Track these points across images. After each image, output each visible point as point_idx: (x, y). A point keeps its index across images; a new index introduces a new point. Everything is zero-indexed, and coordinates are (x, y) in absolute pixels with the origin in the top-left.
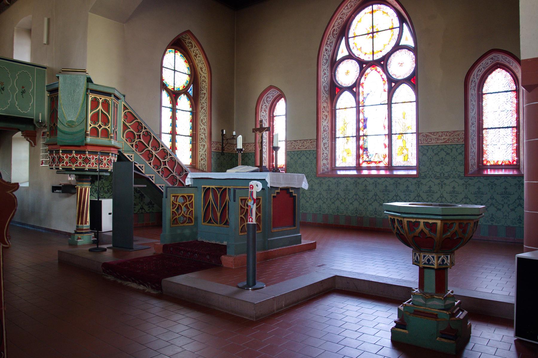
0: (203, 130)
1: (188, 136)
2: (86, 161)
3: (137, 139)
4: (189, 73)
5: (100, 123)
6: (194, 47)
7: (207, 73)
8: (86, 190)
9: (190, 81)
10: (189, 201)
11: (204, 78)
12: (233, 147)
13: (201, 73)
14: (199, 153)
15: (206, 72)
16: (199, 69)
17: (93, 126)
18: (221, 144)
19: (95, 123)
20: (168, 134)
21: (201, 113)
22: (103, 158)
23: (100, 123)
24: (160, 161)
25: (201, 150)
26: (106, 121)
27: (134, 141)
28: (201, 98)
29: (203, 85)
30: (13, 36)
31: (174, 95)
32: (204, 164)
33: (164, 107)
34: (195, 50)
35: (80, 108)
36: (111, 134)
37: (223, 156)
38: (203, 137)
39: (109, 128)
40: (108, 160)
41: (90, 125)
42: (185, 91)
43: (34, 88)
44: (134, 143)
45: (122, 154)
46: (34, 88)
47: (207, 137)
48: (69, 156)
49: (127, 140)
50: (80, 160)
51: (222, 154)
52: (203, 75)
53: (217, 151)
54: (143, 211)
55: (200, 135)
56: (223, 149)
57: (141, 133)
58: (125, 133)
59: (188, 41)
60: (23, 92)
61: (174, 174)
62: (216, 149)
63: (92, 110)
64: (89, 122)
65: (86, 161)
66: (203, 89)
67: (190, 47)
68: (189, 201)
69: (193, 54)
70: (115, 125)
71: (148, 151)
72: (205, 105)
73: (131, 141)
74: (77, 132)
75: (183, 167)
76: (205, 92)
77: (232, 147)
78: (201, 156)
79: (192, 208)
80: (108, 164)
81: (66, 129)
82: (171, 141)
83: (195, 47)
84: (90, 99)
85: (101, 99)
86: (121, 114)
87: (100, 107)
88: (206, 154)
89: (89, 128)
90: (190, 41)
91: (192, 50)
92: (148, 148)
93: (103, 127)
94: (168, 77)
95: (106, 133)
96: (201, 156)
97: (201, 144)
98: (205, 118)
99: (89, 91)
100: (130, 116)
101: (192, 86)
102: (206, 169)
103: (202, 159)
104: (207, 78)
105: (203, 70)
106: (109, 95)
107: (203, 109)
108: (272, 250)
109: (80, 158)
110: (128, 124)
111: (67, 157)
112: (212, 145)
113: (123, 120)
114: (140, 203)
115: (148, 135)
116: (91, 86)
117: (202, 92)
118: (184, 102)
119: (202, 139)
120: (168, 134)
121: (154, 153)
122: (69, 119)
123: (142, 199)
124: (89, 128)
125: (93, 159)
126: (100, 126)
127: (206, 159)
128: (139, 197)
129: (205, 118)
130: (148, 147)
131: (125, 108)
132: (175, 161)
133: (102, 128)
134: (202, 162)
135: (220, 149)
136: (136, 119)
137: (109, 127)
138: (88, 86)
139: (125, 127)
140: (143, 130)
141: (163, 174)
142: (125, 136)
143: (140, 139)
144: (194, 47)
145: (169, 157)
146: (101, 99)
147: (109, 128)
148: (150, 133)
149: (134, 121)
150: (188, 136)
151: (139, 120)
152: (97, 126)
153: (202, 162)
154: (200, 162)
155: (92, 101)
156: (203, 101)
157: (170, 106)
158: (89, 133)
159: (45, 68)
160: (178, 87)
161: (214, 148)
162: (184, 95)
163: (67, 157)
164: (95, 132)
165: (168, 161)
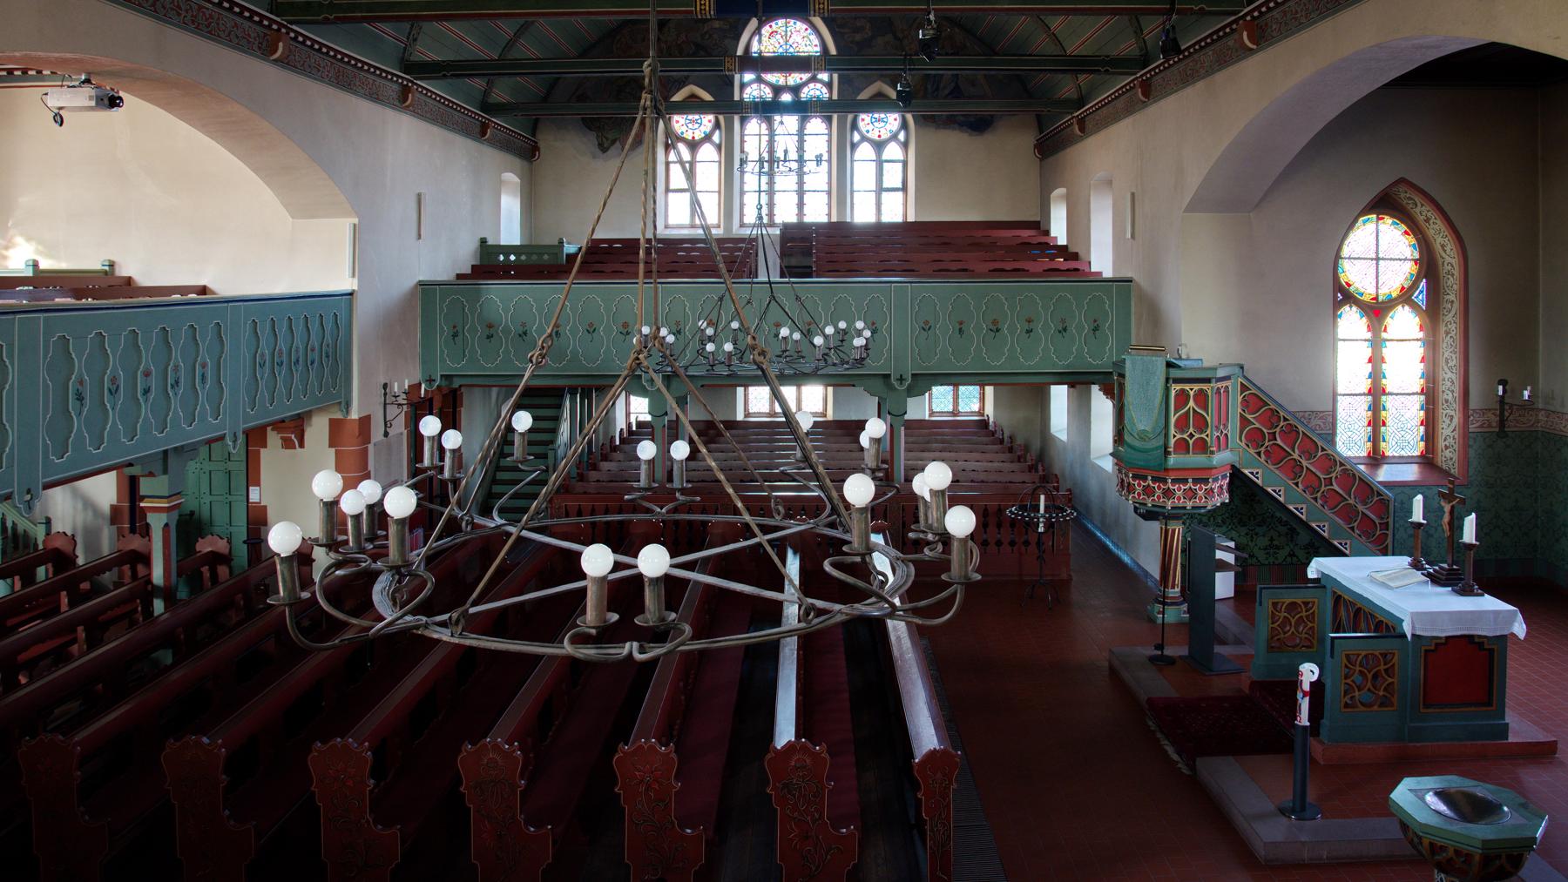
0: (1449, 384)
1: (1413, 394)
2: (1168, 494)
3: (1269, 441)
4: (1416, 255)
5: (1191, 430)
6: (1419, 205)
7: (1456, 256)
8: (1174, 531)
9: (1419, 273)
10: (1306, 611)
11: (1449, 268)
12: (1536, 415)
13: (1444, 255)
14: (1441, 431)
15: (1454, 253)
16: (1438, 247)
17: (1178, 436)
18: (1498, 412)
19: (1182, 432)
20: (1364, 394)
21: (1445, 345)
22: (1175, 488)
23: (1191, 430)
24: (1319, 478)
25: (1445, 426)
26: (1202, 425)
27: (1262, 446)
28: (1445, 311)
29: (1449, 282)
30: (1089, 196)
31: (1376, 311)
32: (1451, 459)
33: (1344, 340)
34: (1422, 211)
35: (1156, 411)
36: (1211, 447)
37: (1504, 440)
38: (1450, 397)
39: (1207, 436)
40: (1206, 490)
41: (1174, 436)
42: (1405, 297)
43: (1112, 319)
44: (1263, 449)
45: (1239, 470)
46: (1112, 319)
47: (1457, 400)
48: (1143, 484)
49: (1248, 446)
50: (1159, 492)
51: (1502, 431)
52: (1448, 259)
53: (1479, 430)
54: (1295, 559)
55: (1443, 392)
56: (1502, 423)
57: (1278, 429)
58: (1245, 432)
59: (1404, 194)
60: (1096, 329)
61: (1351, 501)
62: (1481, 426)
63: (1176, 410)
64: (1172, 430)
65: (1168, 494)
66: (1448, 291)
67: (1411, 206)
68: (1306, 611)
69: (1421, 219)
70: (1222, 420)
71: (1292, 462)
72: (1453, 328)
73: (1257, 446)
74: (1153, 450)
75: (1373, 486)
76: (1452, 297)
77: (1531, 415)
78: (1445, 440)
79: (1314, 622)
80: (1206, 498)
81: (1137, 444)
82: (1369, 409)
83: (1422, 205)
84: (1173, 393)
85: (1191, 389)
86: (1235, 399)
87: (1191, 404)
88: (1456, 436)
89: (1172, 441)
90: (1408, 195)
91: (1418, 210)
92: (1292, 455)
93: (1197, 436)
94: (1357, 275)
95: (1202, 447)
96: (1445, 440)
97: (1445, 412)
98: (1454, 356)
99: (1171, 381)
100: (1255, 400)
101: (1423, 283)
102: (1456, 470)
103: (1446, 447)
104: (1456, 267)
105: (1448, 249)
106: (1208, 381)
107: (1449, 335)
108: (1418, 744)
109: (1159, 488)
110: (1249, 417)
111: (1139, 485)
112: (1472, 418)
113: (1239, 410)
114: (1287, 545)
115: (1291, 432)
116: (1174, 373)
117: (1448, 297)
118: (1404, 323)
119: (1447, 401)
120: (1364, 394)
121: (1305, 463)
122: (1141, 427)
123: (1292, 537)
124: (1172, 441)
125: (1179, 490)
126: (1191, 436)
127: (1456, 447)
128: (1287, 534)
129: (1454, 356)
130: (1292, 453)
131: (1244, 388)
132: (1354, 475)
133: (1194, 438)
134: (1447, 453)
135: (1494, 424)
136: (1266, 404)
137: (1210, 435)
138: (1168, 373)
139: (1244, 422)
140: (1282, 424)
141: (1326, 502)
142: (1243, 438)
143: (1276, 440)
144: (1419, 205)
145: (1339, 469)
146: (1191, 389)
147: (1207, 436)
148: (1296, 427)
149: (1264, 409)
150: (1413, 394)
151: (1272, 407)
152: (1185, 436)
153: (1447, 453)
154: (1442, 451)
155: (1176, 396)
156: (1449, 318)
157: (1369, 335)
158: (1171, 450)
159: (1131, 281)
160: (1387, 291)
161: (1478, 424)
162: (1403, 307)
163: (1139, 485)
164: (1182, 446)
165: (1336, 477)
